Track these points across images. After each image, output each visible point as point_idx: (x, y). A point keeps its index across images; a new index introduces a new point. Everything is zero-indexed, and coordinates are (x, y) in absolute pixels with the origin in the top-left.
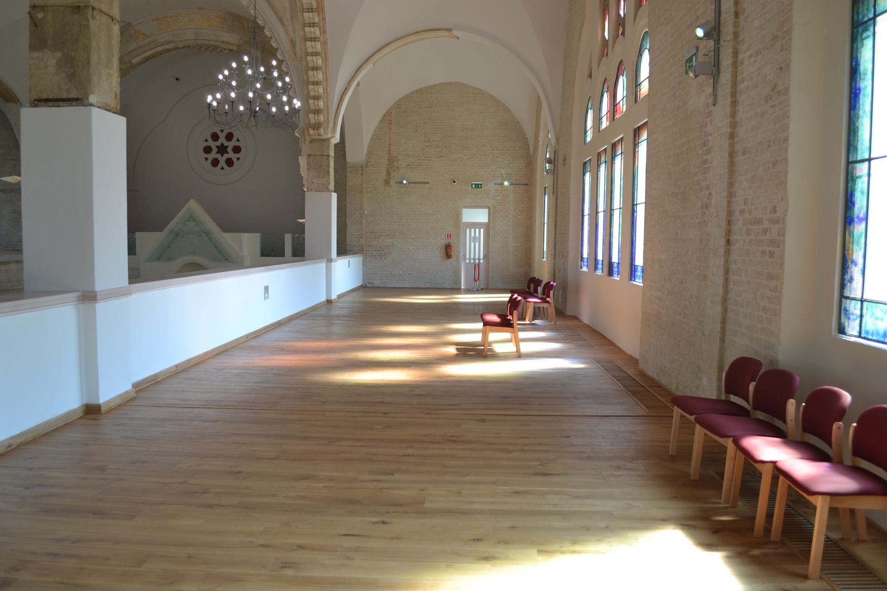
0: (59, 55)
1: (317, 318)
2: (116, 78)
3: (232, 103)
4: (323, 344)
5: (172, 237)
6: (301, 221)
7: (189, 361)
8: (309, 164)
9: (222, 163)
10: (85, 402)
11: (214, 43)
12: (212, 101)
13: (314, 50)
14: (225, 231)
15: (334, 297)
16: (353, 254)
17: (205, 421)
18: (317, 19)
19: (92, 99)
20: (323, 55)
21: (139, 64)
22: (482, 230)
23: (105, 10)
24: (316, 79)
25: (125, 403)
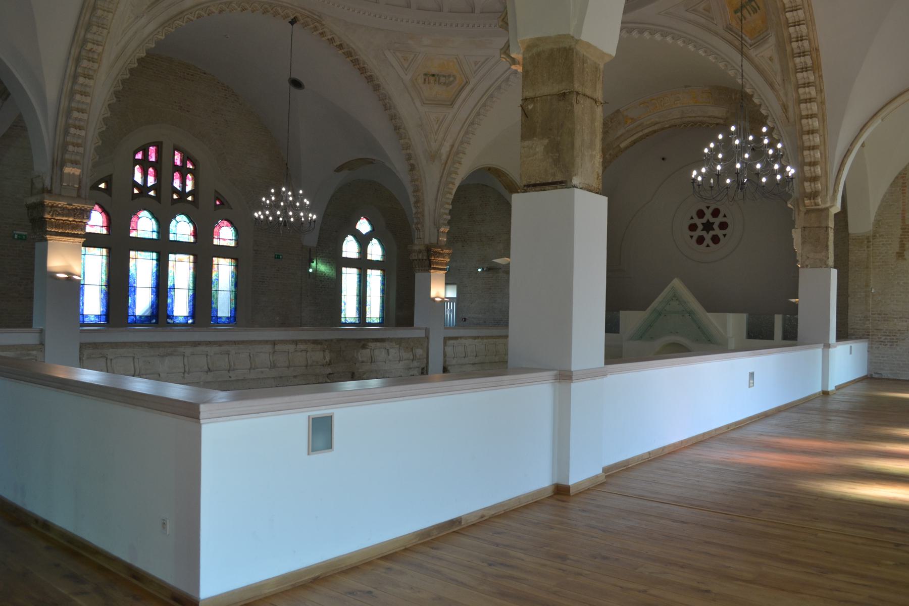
0: (546, 141)
1: (808, 413)
2: (598, 159)
3: (719, 176)
4: (817, 444)
5: (651, 318)
6: (793, 300)
7: (664, 448)
8: (803, 237)
9: (708, 240)
10: (555, 482)
11: (701, 119)
12: (697, 176)
13: (810, 112)
14: (709, 311)
15: (831, 388)
16: (857, 338)
17: (674, 521)
18: (812, 78)
19: (576, 181)
20: (820, 116)
21: (627, 148)
22: (349, 312)
23: (588, 92)
24: (812, 144)
25: (594, 487)
